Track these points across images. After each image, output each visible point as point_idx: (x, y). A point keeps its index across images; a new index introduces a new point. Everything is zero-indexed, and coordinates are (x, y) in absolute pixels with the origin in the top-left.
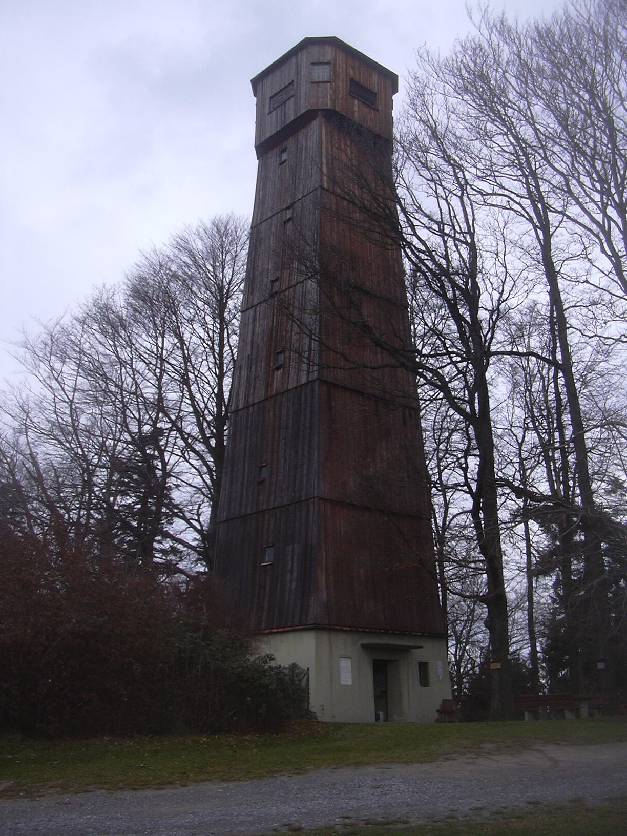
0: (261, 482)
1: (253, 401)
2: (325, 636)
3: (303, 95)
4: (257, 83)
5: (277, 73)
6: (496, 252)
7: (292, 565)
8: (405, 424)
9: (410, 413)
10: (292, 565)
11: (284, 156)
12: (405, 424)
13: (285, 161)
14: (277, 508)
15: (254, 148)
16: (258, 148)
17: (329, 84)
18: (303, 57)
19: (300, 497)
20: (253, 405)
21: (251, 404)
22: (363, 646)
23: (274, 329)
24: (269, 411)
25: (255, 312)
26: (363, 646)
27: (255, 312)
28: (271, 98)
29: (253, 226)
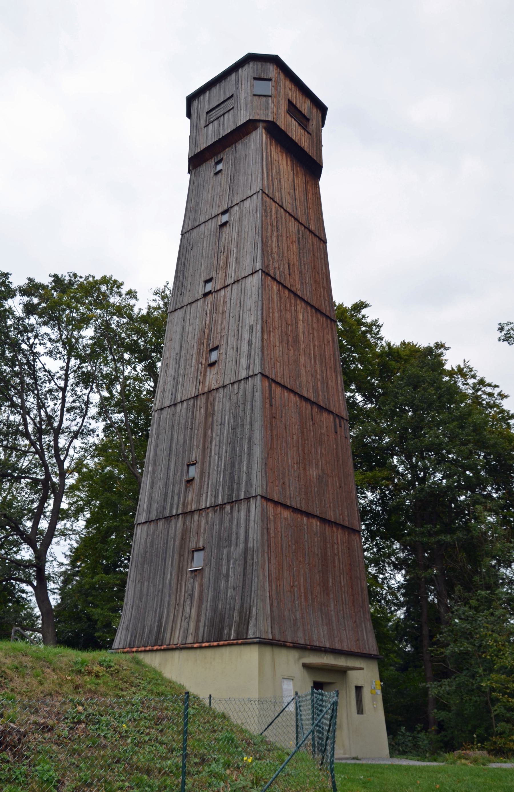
0: (190, 481)
1: (181, 397)
2: (268, 651)
3: (243, 98)
4: (191, 100)
5: (215, 90)
6: (273, 701)
7: (228, 570)
8: (336, 432)
9: (340, 422)
10: (228, 570)
11: (219, 167)
12: (336, 432)
13: (221, 171)
14: (208, 508)
15: (187, 160)
16: (191, 160)
17: (270, 98)
18: (245, 72)
19: (238, 495)
20: (182, 402)
21: (179, 401)
22: (305, 666)
23: (207, 327)
24: (200, 408)
25: (185, 314)
26: (305, 666)
27: (185, 314)
28: (208, 113)
29: (184, 231)
